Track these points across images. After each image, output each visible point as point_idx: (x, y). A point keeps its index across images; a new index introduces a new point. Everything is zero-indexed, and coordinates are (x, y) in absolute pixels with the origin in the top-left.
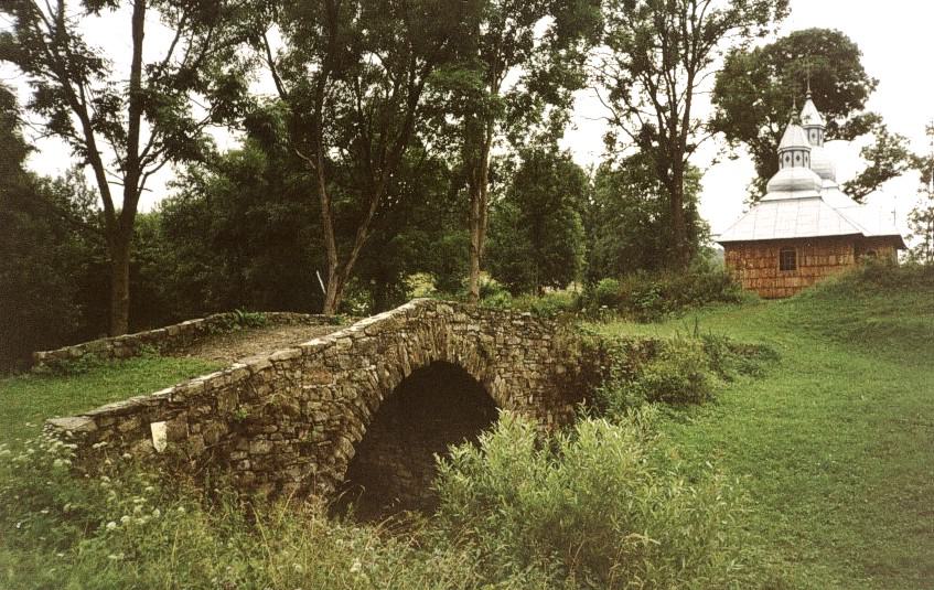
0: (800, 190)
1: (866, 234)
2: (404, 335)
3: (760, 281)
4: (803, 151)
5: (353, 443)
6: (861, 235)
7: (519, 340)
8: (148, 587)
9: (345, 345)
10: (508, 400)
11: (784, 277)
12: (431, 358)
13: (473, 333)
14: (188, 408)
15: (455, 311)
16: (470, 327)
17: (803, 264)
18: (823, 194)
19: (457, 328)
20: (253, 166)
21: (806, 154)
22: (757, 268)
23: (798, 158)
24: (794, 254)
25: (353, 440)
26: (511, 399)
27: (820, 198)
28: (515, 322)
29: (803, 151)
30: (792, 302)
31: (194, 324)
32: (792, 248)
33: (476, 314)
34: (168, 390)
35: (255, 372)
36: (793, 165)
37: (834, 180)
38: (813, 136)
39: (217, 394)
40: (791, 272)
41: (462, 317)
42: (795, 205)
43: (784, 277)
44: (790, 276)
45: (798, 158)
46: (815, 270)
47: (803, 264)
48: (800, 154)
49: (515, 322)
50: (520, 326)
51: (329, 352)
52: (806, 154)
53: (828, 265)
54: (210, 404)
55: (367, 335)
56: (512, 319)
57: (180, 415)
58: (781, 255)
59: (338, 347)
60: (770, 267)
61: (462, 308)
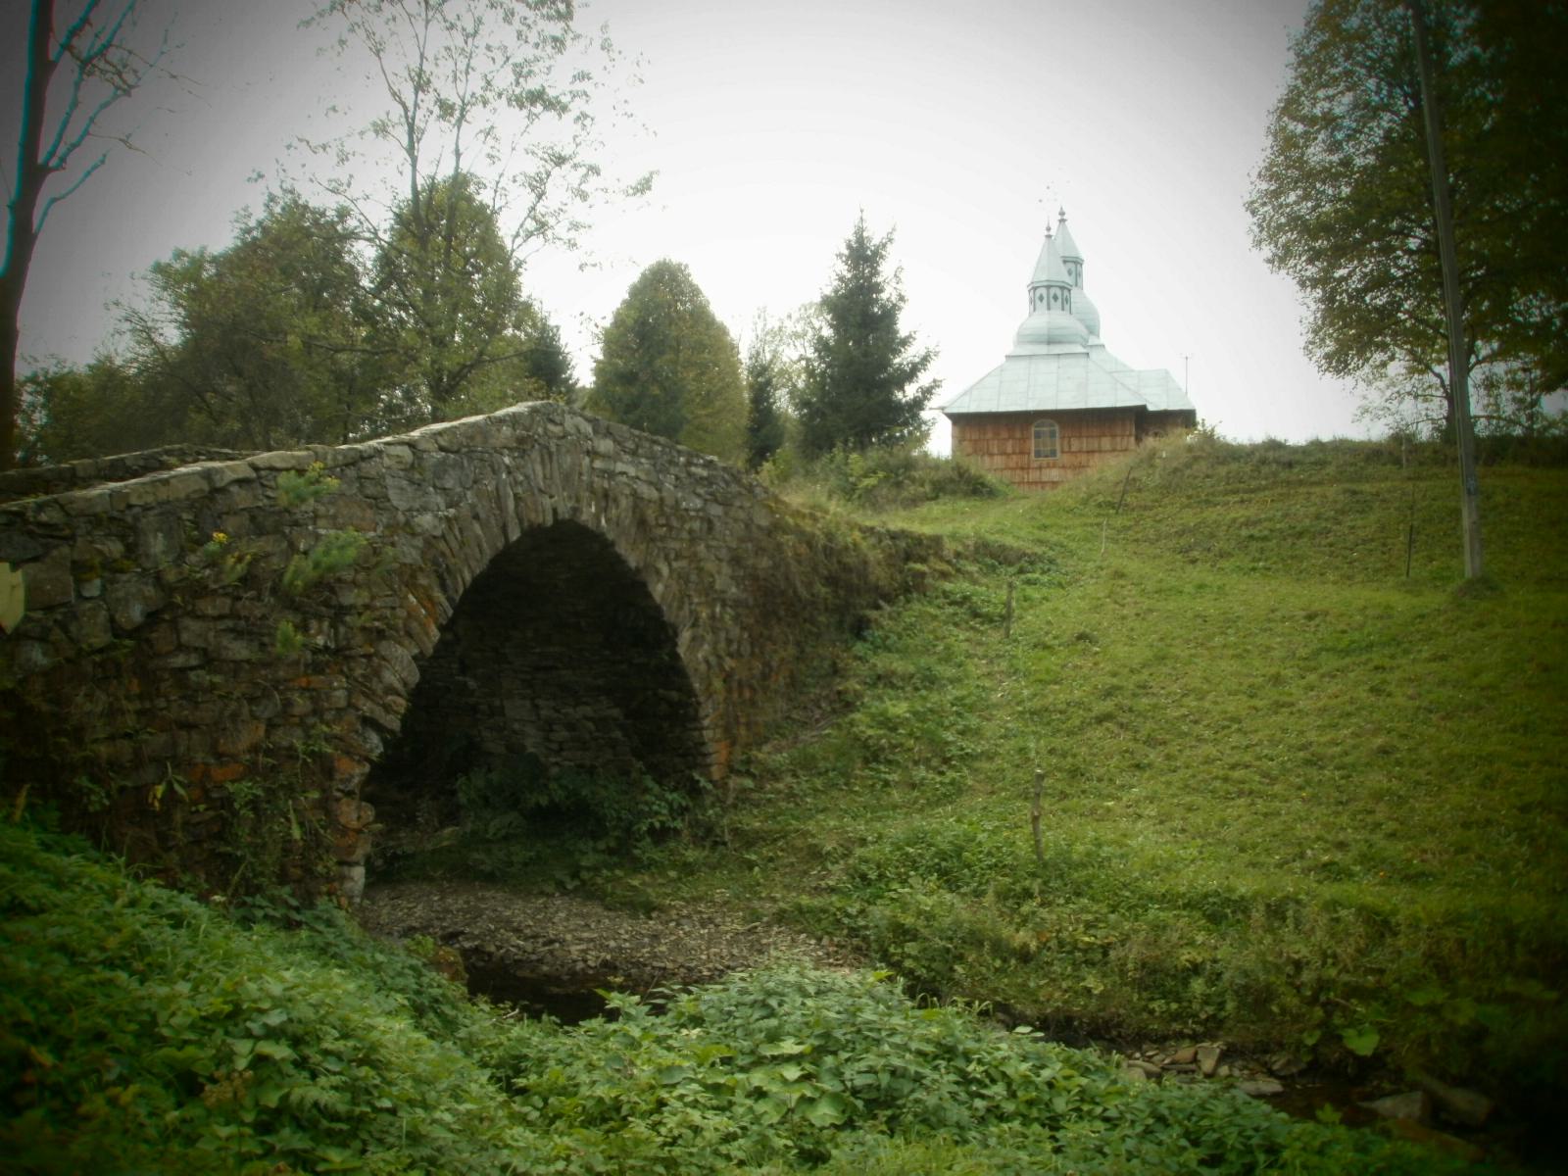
0: (1060, 342)
1: (1151, 408)
2: (507, 460)
4: (1062, 288)
5: (415, 658)
6: (1144, 407)
7: (699, 503)
8: (908, 1173)
9: (399, 458)
10: (680, 608)
12: (555, 511)
13: (624, 479)
14: (70, 539)
15: (596, 432)
16: (620, 467)
19: (598, 464)
22: (1003, 453)
25: (416, 651)
26: (686, 607)
28: (693, 469)
29: (1062, 288)
31: (123, 459)
34: (183, 470)
35: (219, 484)
36: (1049, 308)
39: (136, 518)
41: (605, 445)
42: (1053, 365)
44: (1048, 466)
45: (1055, 298)
46: (1083, 458)
48: (1059, 292)
49: (693, 469)
51: (369, 468)
52: (1066, 293)
54: (122, 538)
55: (442, 449)
56: (689, 463)
57: (55, 553)
59: (387, 461)
60: (1022, 453)
61: (608, 428)
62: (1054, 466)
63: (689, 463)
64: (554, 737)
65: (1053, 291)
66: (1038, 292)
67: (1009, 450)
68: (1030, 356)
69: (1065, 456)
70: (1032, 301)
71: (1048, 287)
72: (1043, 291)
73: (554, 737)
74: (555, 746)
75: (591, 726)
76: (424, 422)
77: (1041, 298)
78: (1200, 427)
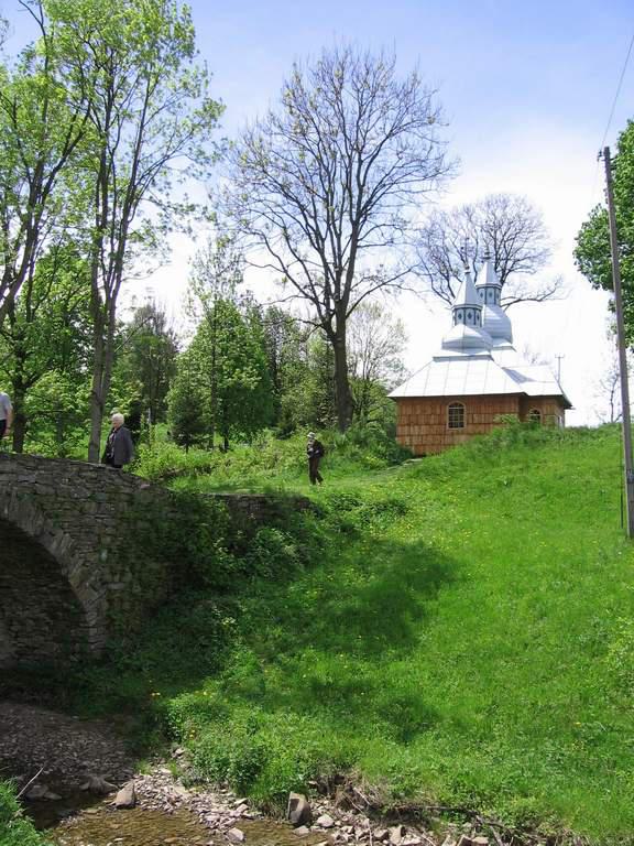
1: (530, 394)
3: (430, 438)
11: (452, 434)
16: (22, 478)
17: (471, 421)
18: (494, 354)
20: (248, 378)
21: (497, 291)
23: (470, 316)
24: (462, 410)
27: (511, 348)
30: (98, 190)
32: (461, 405)
33: (32, 464)
37: (510, 340)
38: (491, 295)
40: (460, 429)
43: (452, 434)
44: (458, 433)
45: (470, 316)
46: (481, 428)
47: (471, 421)
48: (472, 312)
49: (84, 474)
50: (92, 479)
52: (497, 291)
53: (494, 423)
58: (450, 412)
62: (463, 433)
63: (80, 470)
64: (13, 628)
65: (468, 311)
66: (459, 312)
67: (432, 422)
68: (450, 359)
69: (470, 427)
70: (455, 318)
71: (487, 288)
72: (461, 311)
73: (13, 628)
74: (14, 635)
75: (31, 622)
76: (95, 291)
77: (460, 316)
78: (414, 625)
